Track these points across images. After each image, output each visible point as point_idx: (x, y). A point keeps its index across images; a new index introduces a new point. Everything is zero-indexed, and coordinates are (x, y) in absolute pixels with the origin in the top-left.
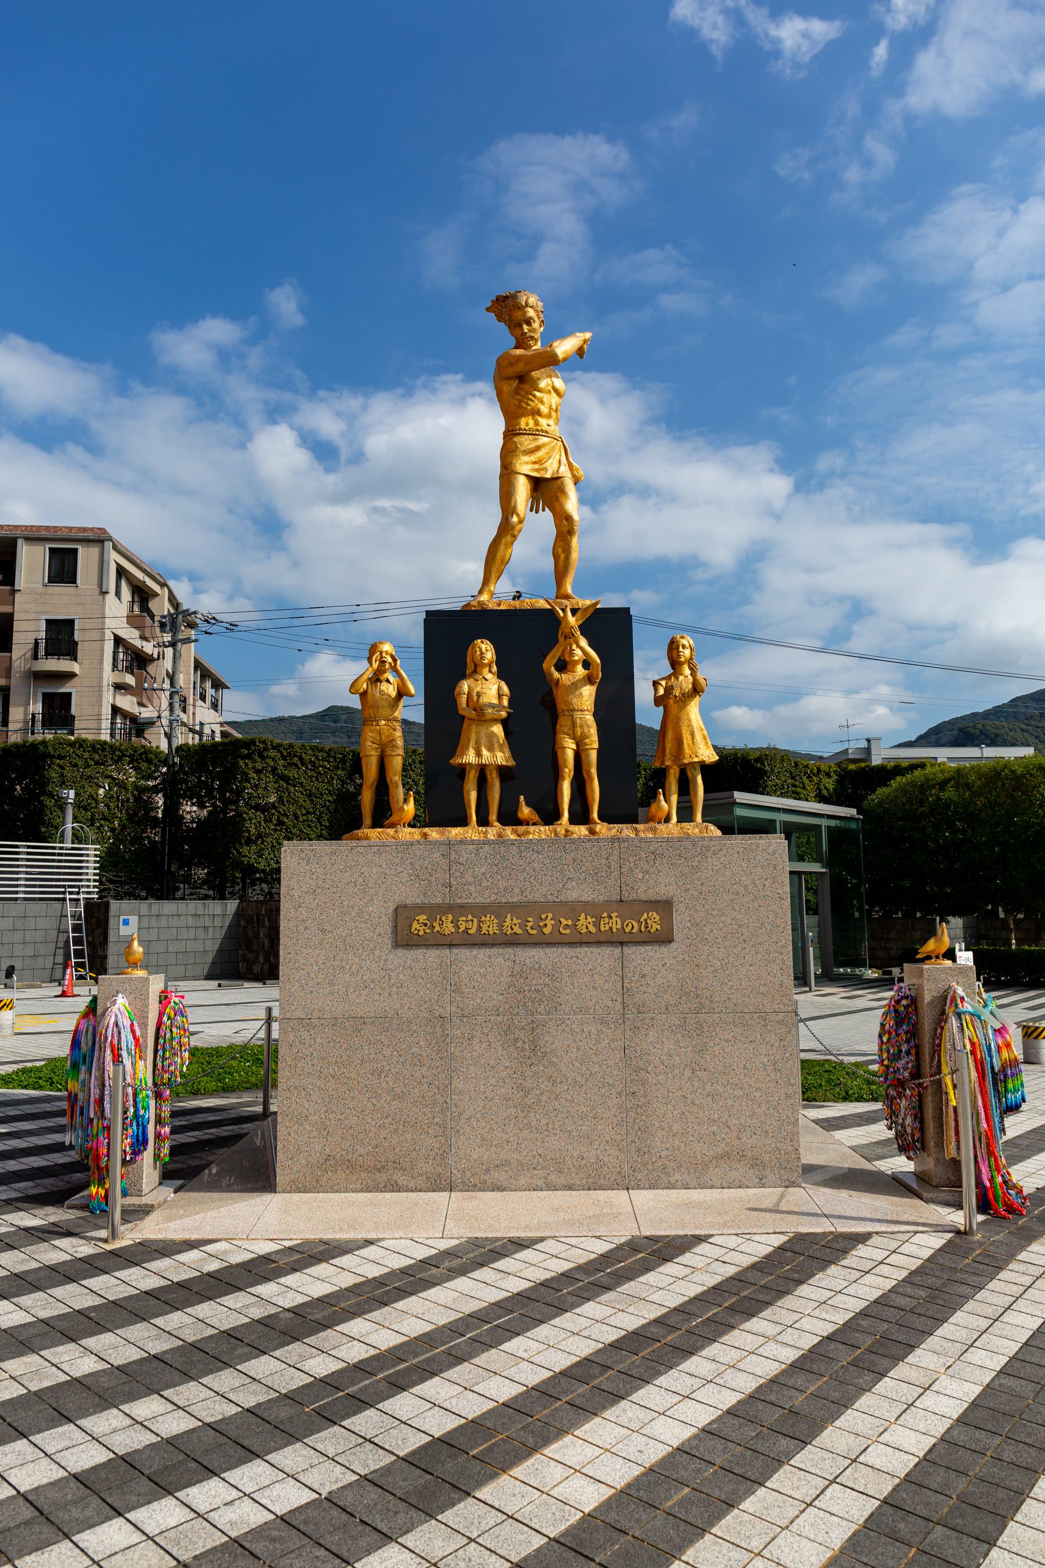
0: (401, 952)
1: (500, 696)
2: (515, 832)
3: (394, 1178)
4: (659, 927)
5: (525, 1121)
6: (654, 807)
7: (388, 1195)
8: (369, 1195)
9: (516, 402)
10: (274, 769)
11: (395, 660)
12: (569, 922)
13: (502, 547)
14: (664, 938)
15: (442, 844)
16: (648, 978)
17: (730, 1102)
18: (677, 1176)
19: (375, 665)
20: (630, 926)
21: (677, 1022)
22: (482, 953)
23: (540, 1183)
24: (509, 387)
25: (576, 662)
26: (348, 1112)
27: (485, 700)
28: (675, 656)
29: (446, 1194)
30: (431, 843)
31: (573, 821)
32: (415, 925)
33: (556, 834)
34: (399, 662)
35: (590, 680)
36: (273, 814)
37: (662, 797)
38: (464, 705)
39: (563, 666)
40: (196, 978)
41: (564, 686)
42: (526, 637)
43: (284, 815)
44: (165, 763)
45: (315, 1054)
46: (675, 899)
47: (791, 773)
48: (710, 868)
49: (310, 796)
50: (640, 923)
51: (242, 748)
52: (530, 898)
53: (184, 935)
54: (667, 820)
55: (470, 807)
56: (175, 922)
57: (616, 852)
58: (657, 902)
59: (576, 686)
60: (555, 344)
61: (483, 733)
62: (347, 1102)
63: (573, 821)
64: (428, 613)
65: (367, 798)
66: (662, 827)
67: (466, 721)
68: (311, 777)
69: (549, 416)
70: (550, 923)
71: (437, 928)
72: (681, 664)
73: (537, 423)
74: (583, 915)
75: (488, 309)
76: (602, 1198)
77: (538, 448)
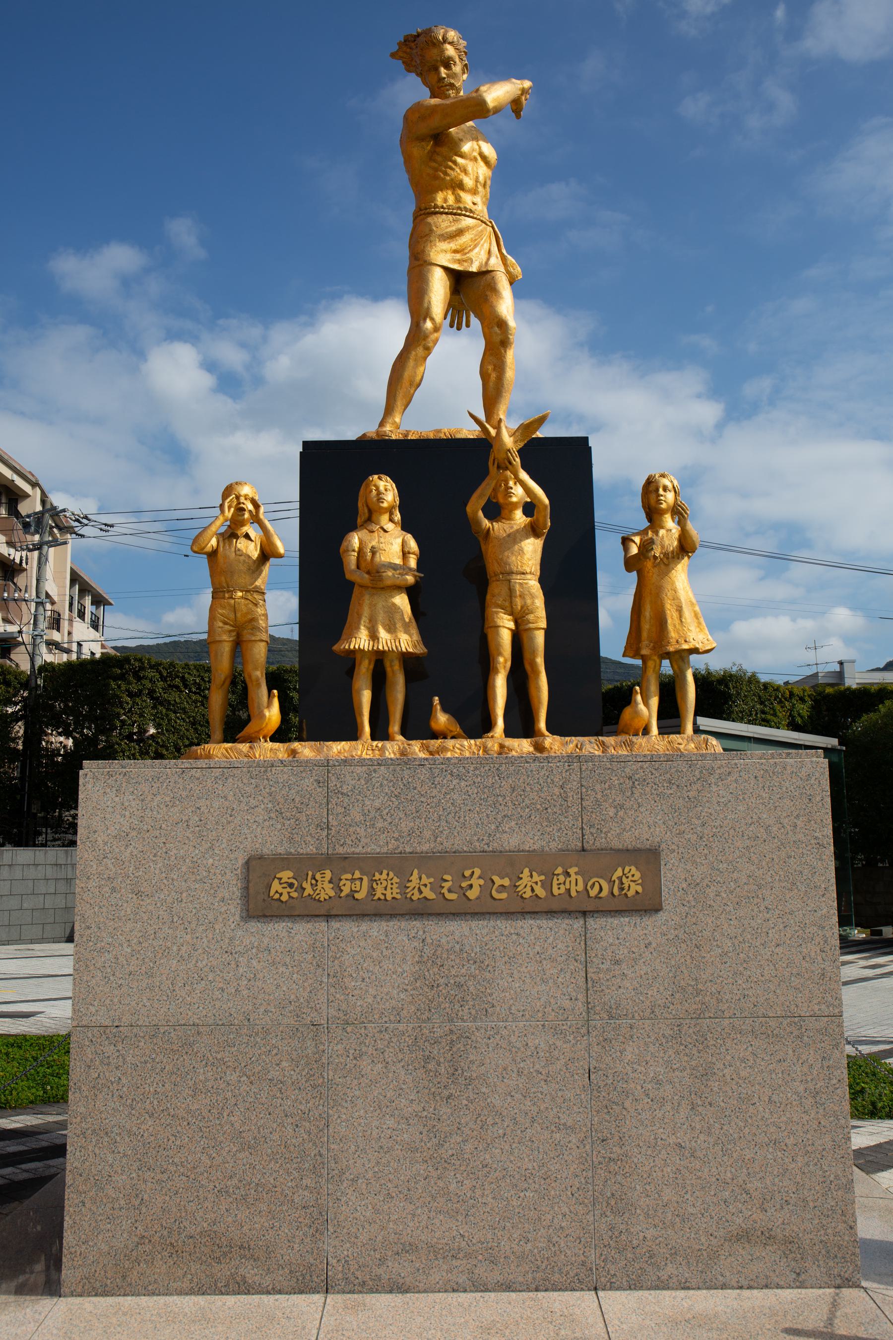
0: (254, 926)
1: (405, 554)
3: (241, 1271)
4: (639, 889)
5: (441, 1184)
6: (627, 713)
7: (231, 1300)
8: (201, 1300)
9: (431, 171)
10: (151, 693)
11: (256, 506)
12: (506, 882)
13: (411, 363)
14: (648, 905)
16: (624, 966)
17: (748, 1154)
18: (670, 1269)
19: (229, 514)
20: (597, 887)
21: (668, 1032)
22: (376, 929)
23: (462, 1279)
24: (420, 151)
25: (515, 506)
26: (173, 1168)
29: (318, 1298)
30: (300, 763)
32: (276, 886)
33: (486, 750)
34: (262, 510)
35: (533, 530)
36: (150, 745)
38: (353, 566)
39: (495, 511)
40: (55, 940)
41: (497, 538)
42: (442, 478)
43: (162, 746)
44: (25, 685)
45: (124, 1081)
46: (663, 846)
47: (760, 697)
49: (193, 724)
50: (611, 883)
52: (447, 845)
53: (42, 888)
54: (646, 731)
55: (361, 714)
56: (32, 873)
57: (575, 777)
58: (637, 851)
59: (514, 538)
62: (171, 1153)
63: (509, 732)
64: (306, 444)
65: (217, 700)
66: (640, 740)
67: (356, 590)
68: (195, 702)
69: (474, 192)
70: (476, 882)
71: (309, 890)
72: (662, 513)
73: (458, 199)
74: (526, 871)
75: (393, 55)
76: (557, 1306)
77: (460, 232)
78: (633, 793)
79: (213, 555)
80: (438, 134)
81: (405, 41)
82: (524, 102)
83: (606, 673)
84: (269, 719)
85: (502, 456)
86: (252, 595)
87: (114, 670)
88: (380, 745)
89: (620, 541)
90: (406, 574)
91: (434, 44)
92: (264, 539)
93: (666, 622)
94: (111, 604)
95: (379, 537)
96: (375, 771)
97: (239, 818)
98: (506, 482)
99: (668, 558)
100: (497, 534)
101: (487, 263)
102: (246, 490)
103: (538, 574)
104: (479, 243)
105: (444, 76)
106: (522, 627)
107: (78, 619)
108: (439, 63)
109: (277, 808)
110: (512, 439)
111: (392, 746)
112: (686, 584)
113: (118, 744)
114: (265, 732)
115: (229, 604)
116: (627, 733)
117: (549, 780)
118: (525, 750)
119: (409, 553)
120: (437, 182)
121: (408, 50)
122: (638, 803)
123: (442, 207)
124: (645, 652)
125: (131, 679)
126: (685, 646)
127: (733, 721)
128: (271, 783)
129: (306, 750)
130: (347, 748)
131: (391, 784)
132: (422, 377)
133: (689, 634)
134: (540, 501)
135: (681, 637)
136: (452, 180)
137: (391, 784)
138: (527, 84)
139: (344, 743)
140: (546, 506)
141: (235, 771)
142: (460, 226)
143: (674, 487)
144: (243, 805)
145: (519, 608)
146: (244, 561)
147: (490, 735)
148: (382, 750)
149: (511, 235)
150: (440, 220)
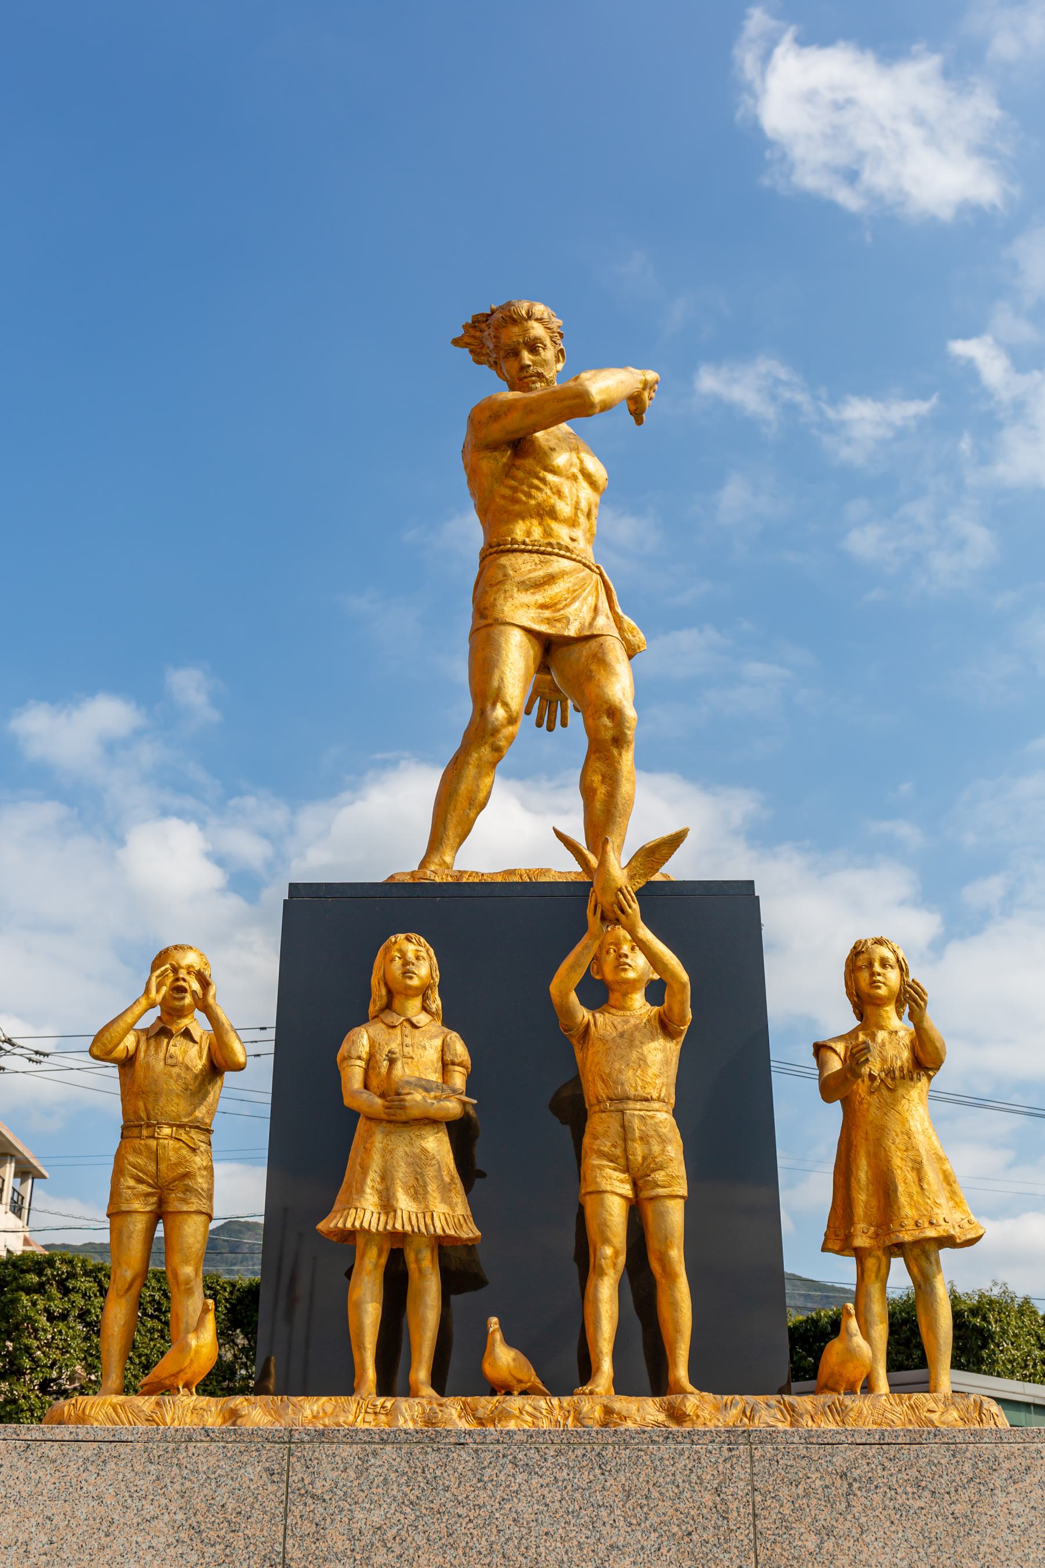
1: (446, 1066)
2: (468, 1411)
6: (834, 1350)
11: (205, 984)
13: (471, 771)
24: (492, 463)
25: (630, 986)
30: (240, 1437)
31: (622, 1386)
33: (579, 1419)
35: (665, 1027)
37: (853, 1324)
39: (598, 992)
41: (603, 1040)
48: (1002, 1521)
54: (868, 1387)
55: (361, 1347)
57: (741, 1472)
59: (628, 1039)
60: (584, 376)
63: (622, 1386)
66: (857, 1403)
67: (361, 1124)
69: (573, 523)
72: (879, 1003)
73: (548, 533)
75: (456, 342)
77: (551, 579)
78: (849, 1505)
80: (519, 440)
81: (474, 322)
82: (648, 402)
83: (793, 1297)
84: (197, 1352)
85: (608, 899)
86: (187, 1133)
87: (28, 1276)
88: (388, 1404)
89: (812, 1050)
90: (447, 1098)
93: (896, 1190)
94: (43, 1177)
96: (375, 1454)
97: (122, 1540)
98: (618, 945)
99: (893, 1079)
101: (591, 624)
102: (190, 959)
103: (673, 1101)
104: (580, 595)
105: (528, 362)
106: (645, 1194)
108: (522, 346)
109: (193, 1521)
111: (411, 1407)
112: (927, 1124)
113: (24, 1397)
114: (187, 1376)
115: (148, 1147)
118: (650, 1418)
122: (861, 1526)
124: (861, 1241)
126: (931, 1233)
127: (999, 1375)
129: (256, 1413)
133: (936, 1210)
134: (674, 975)
135: (922, 1216)
136: (539, 505)
139: (324, 1399)
141: (122, 1449)
142: (550, 570)
143: (898, 961)
144: (130, 1514)
145: (640, 1159)
146: (179, 1075)
147: (587, 1389)
150: (520, 561)
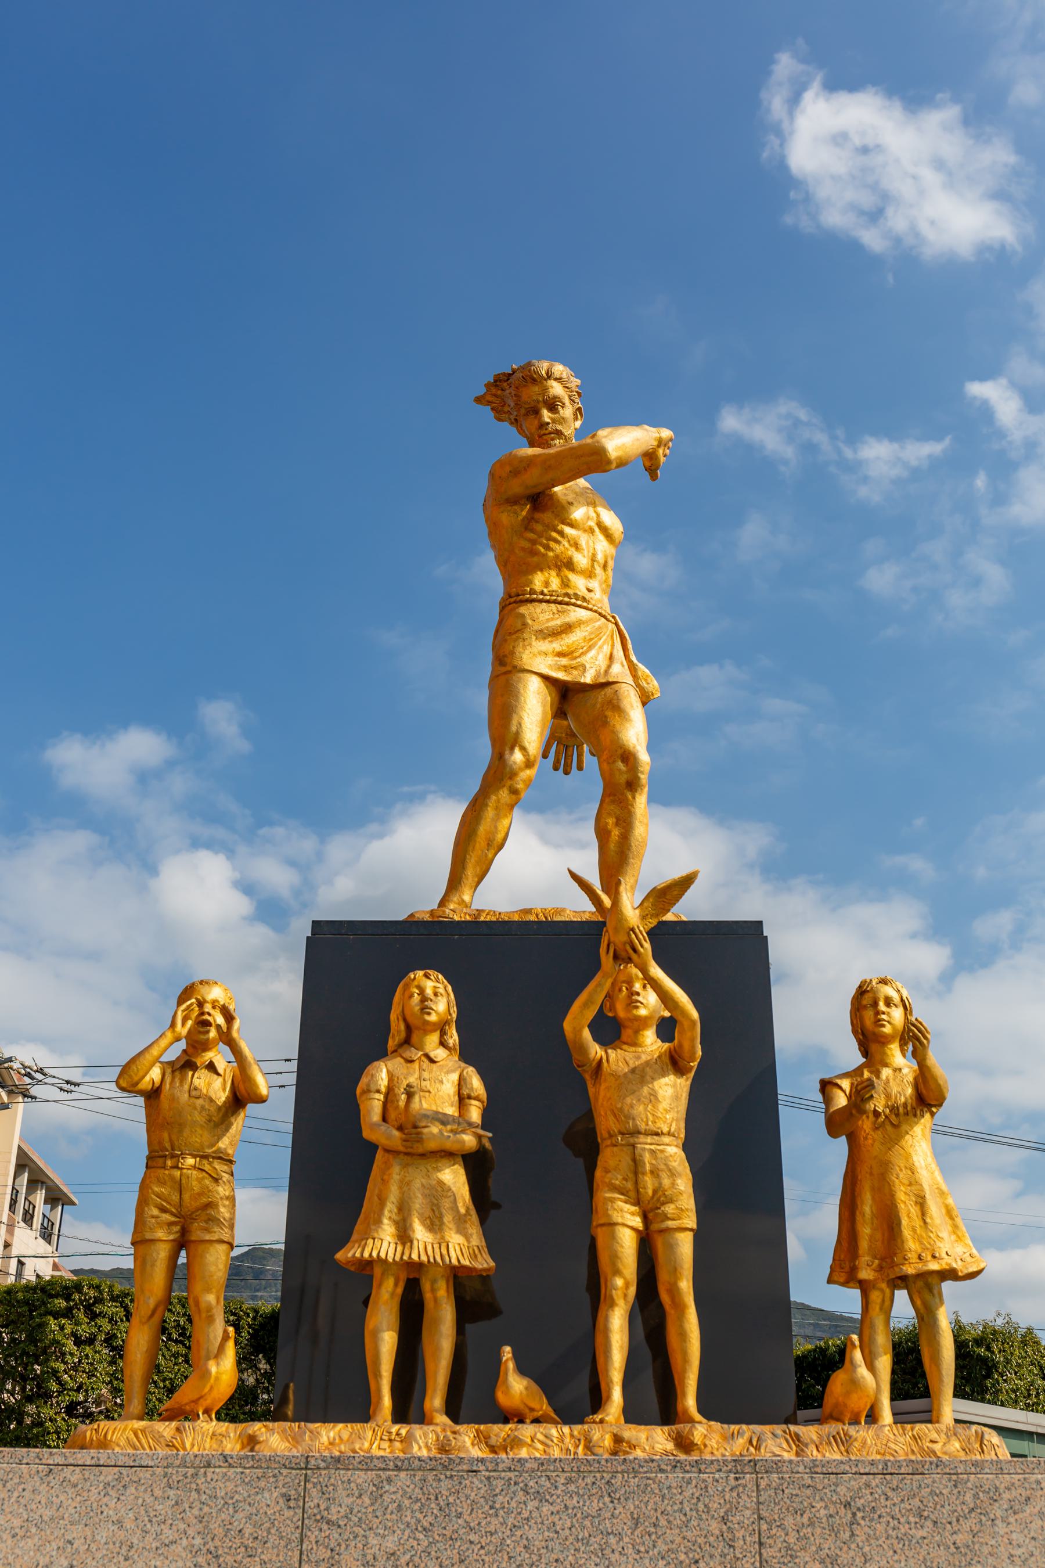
1: (463, 1099)
2: (482, 1439)
6: (838, 1381)
9: (527, 545)
11: (229, 1018)
13: (490, 813)
15: (288, 1464)
25: (642, 1023)
27: (422, 1104)
28: (869, 1022)
31: (632, 1415)
33: (589, 1447)
34: (236, 1024)
35: (675, 1063)
37: (858, 1355)
38: (376, 1116)
39: (611, 1029)
41: (615, 1075)
51: (57, 1296)
54: (872, 1417)
55: (378, 1375)
57: (748, 1501)
59: (641, 1075)
61: (417, 1184)
63: (632, 1415)
66: (861, 1433)
67: (380, 1155)
68: (176, 1355)
69: (590, 574)
72: (883, 1041)
73: (565, 583)
75: (478, 400)
78: (853, 1535)
79: (152, 1095)
80: (538, 495)
81: (495, 381)
82: (662, 459)
84: (217, 1379)
85: (620, 939)
86: (210, 1163)
87: (56, 1301)
88: (403, 1432)
89: (818, 1086)
90: (463, 1132)
91: (534, 380)
92: (238, 1072)
93: (899, 1224)
94: (73, 1204)
95: (421, 1070)
96: (389, 1480)
98: (630, 983)
99: (897, 1115)
100: (614, 1067)
101: (606, 672)
102: (215, 993)
103: (683, 1135)
105: (547, 420)
106: (655, 1227)
107: (22, 1224)
108: (541, 405)
109: (211, 1545)
110: (637, 911)
111: (425, 1435)
113: (51, 1420)
115: (172, 1178)
116: (839, 1419)
117: (701, 1506)
118: (659, 1447)
119: (469, 1097)
120: (535, 559)
121: (499, 392)
122: (864, 1555)
123: (542, 593)
125: (81, 1316)
126: (934, 1266)
127: (1002, 1405)
128: (204, 1497)
129: (274, 1438)
130: (345, 1436)
131: (417, 1507)
132: (507, 834)
133: (939, 1244)
134: (684, 1013)
135: (925, 1249)
136: (557, 556)
137: (417, 1507)
138: (666, 433)
139: (341, 1426)
140: (693, 1022)
141: (143, 1474)
143: (902, 1000)
144: (149, 1538)
145: (650, 1192)
146: (203, 1107)
147: (598, 1417)
148: (407, 1440)
149: (644, 641)
150: (538, 611)
